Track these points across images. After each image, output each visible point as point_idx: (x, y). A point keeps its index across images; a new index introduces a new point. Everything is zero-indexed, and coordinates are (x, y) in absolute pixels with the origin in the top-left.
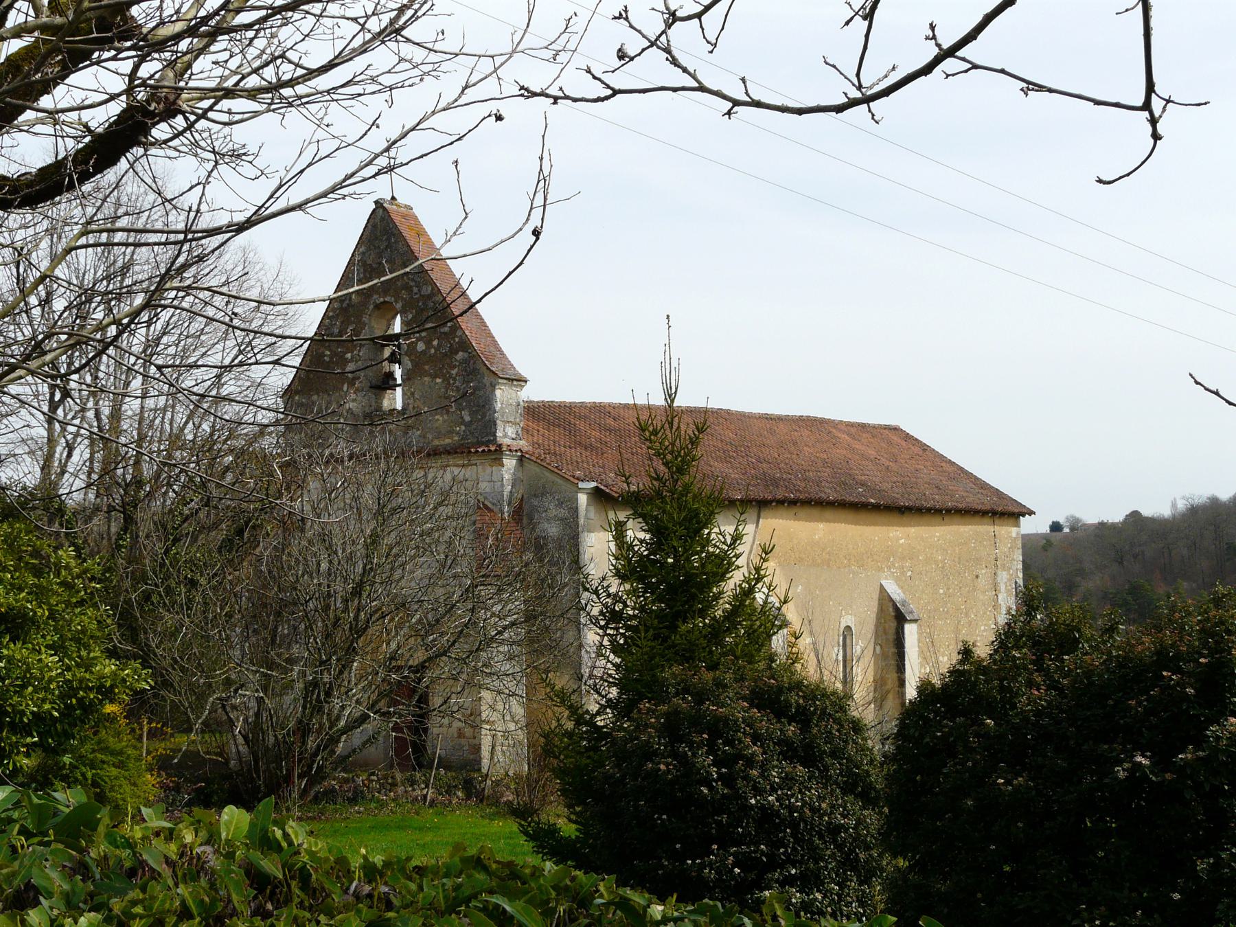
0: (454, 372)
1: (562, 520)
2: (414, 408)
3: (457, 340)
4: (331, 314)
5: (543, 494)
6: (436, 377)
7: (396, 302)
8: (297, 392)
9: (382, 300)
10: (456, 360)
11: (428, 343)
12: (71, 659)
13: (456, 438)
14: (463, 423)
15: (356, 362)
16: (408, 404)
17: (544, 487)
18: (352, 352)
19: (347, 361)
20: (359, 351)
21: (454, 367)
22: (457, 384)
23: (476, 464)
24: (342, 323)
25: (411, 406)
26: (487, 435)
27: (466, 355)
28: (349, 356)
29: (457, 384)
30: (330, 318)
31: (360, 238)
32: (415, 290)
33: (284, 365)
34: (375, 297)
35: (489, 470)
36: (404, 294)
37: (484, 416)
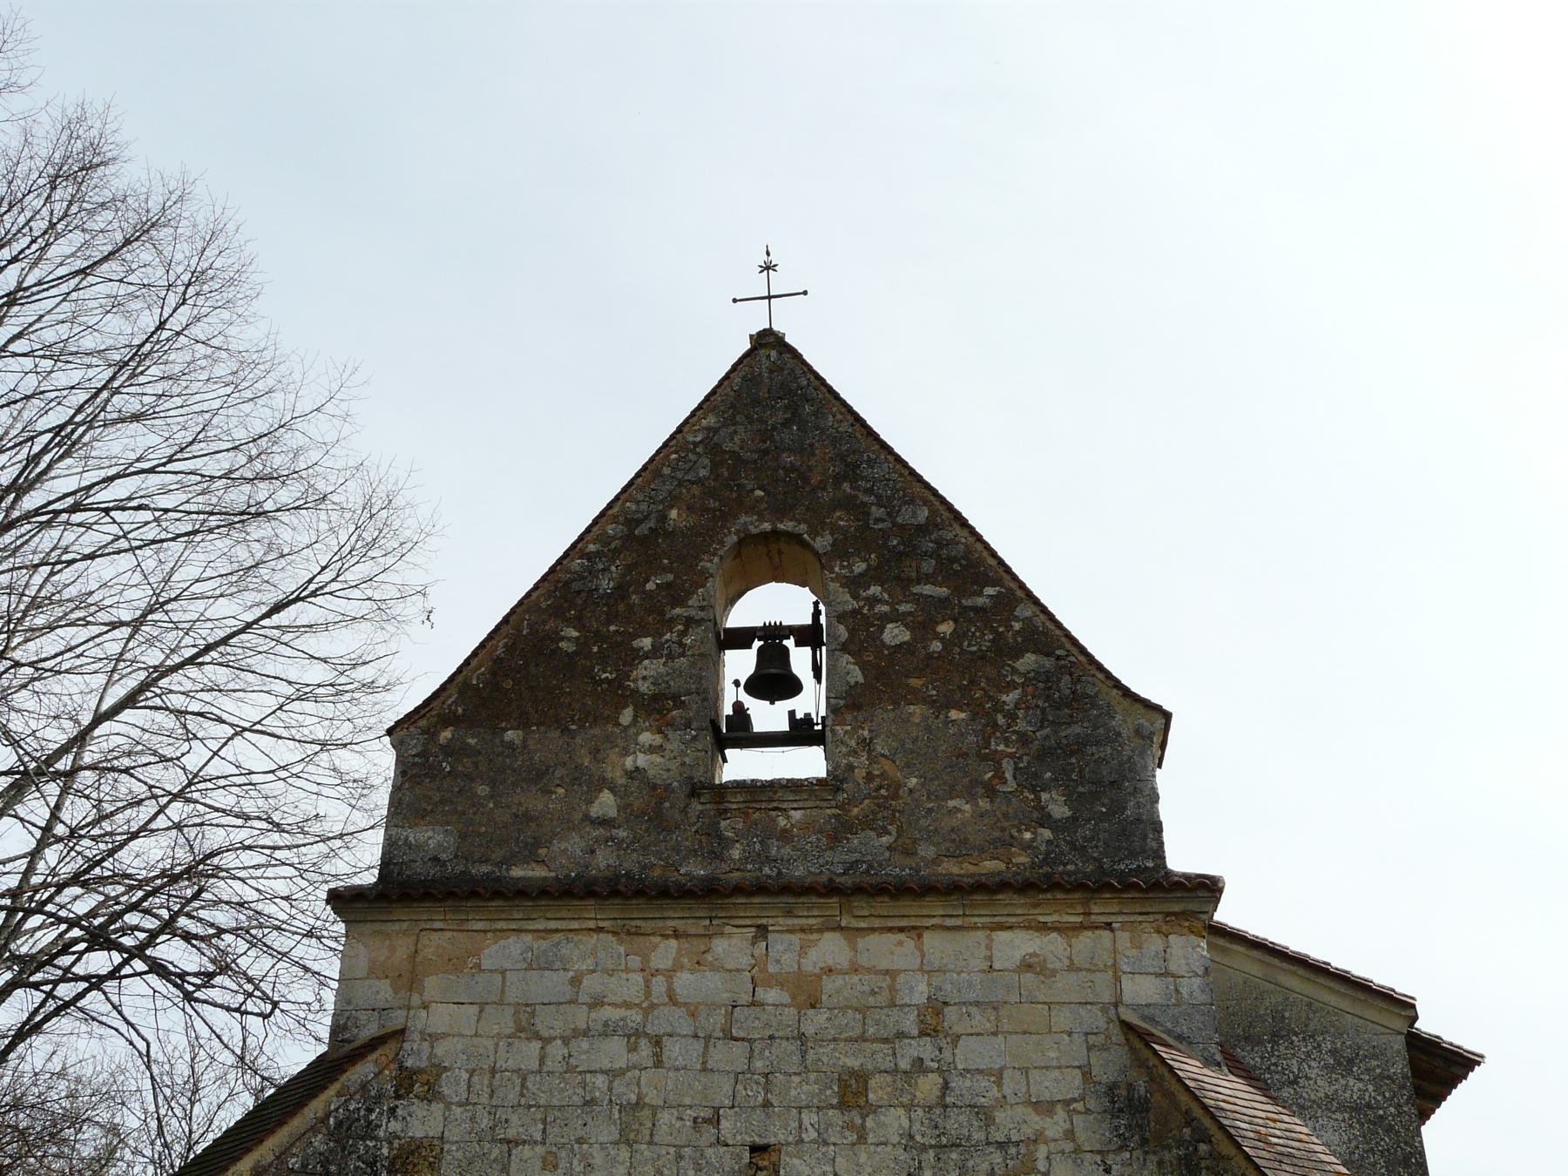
0: (1010, 698)
1: (1356, 1109)
2: (869, 777)
3: (1017, 626)
4: (592, 548)
5: (1275, 1037)
6: (949, 706)
7: (814, 533)
8: (447, 720)
9: (767, 526)
10: (1014, 671)
11: (923, 627)
12: (752, 1091)
13: (1022, 859)
14: (1045, 820)
15: (671, 657)
16: (851, 768)
17: (1278, 1016)
18: (657, 634)
19: (638, 656)
20: (684, 633)
21: (1012, 686)
22: (1021, 726)
23: (1108, 926)
24: (629, 568)
25: (860, 774)
26: (1133, 855)
27: (1048, 663)
28: (646, 642)
29: (1021, 726)
30: (604, 540)
31: (707, 398)
32: (877, 512)
33: (205, 745)
34: (744, 519)
35: (1155, 943)
36: (842, 519)
37: (1118, 807)
